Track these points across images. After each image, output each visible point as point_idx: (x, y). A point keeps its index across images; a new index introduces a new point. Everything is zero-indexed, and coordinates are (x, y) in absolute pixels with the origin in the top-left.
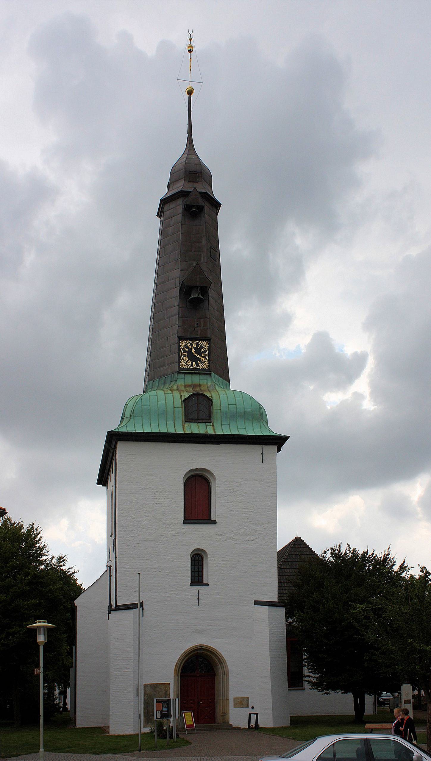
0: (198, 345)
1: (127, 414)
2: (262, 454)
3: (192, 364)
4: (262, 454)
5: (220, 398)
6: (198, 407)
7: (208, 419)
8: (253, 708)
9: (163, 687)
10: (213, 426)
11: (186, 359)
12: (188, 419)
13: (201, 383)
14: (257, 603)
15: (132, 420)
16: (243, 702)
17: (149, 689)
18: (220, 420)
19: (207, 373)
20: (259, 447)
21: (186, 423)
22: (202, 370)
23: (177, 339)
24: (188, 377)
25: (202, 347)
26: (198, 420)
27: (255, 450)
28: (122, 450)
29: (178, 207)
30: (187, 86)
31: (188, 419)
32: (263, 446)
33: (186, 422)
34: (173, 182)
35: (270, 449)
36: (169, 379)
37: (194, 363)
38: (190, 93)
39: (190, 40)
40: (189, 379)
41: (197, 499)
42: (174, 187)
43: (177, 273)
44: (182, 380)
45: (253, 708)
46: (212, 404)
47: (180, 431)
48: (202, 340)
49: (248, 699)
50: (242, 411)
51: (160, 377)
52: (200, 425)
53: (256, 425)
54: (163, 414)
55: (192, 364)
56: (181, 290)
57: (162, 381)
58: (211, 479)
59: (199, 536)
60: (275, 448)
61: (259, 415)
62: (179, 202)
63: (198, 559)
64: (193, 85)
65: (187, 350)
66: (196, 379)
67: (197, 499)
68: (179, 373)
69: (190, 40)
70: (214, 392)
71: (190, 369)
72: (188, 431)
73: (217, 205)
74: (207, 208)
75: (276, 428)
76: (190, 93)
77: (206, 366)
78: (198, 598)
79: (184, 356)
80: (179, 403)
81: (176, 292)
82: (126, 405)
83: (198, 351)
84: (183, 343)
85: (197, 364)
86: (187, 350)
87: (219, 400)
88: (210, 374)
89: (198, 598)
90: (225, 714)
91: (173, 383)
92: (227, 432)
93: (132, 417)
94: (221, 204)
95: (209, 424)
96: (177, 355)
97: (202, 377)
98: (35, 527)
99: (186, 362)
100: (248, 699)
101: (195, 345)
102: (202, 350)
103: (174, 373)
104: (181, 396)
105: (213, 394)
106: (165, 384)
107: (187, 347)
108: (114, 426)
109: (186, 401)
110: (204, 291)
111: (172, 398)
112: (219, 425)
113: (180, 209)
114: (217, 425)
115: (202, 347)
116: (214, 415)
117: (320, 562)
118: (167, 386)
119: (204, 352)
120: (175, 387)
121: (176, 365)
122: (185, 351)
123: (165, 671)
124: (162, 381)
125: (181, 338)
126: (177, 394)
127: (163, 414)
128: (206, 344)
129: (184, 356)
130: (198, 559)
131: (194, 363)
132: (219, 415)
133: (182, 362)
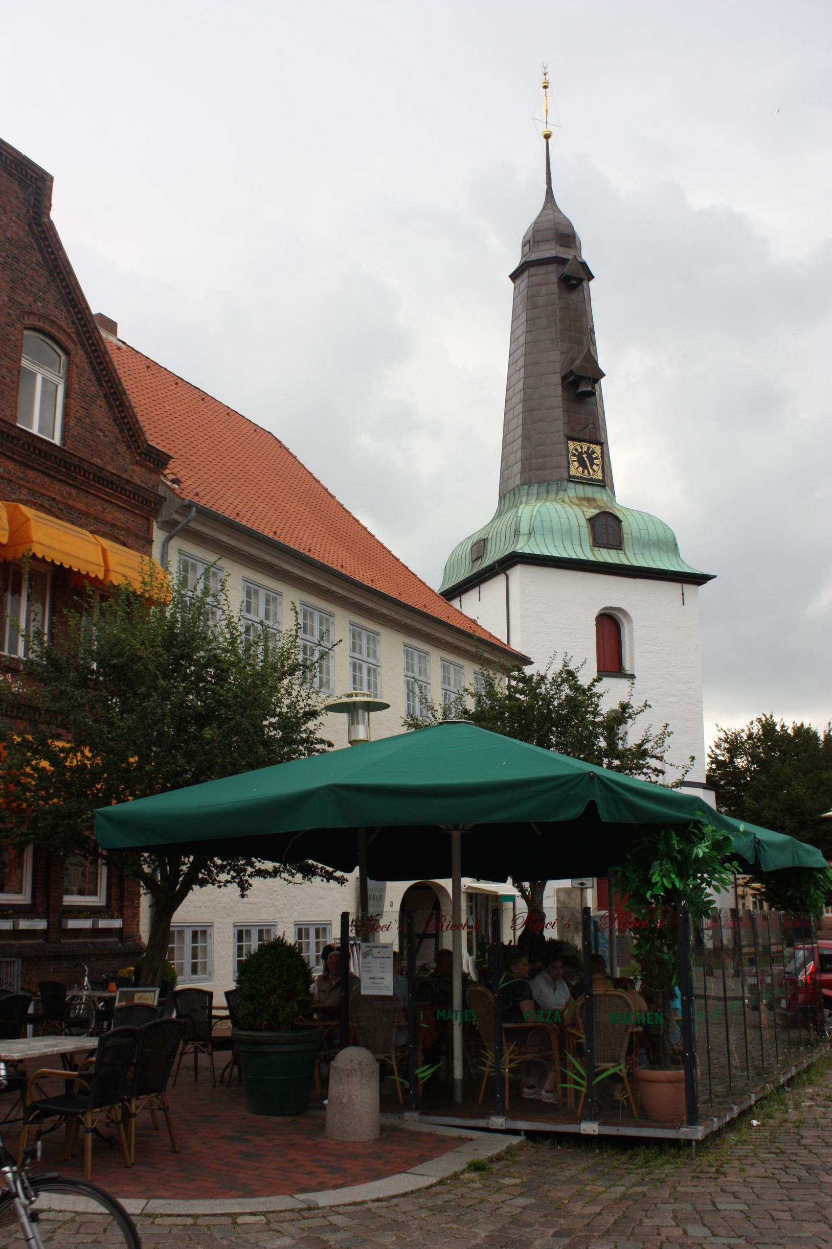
0: (588, 448)
2: (683, 594)
4: (683, 594)
7: (617, 544)
11: (576, 464)
12: (597, 543)
15: (532, 538)
17: (562, 894)
23: (563, 439)
24: (580, 487)
25: (593, 452)
27: (674, 588)
30: (543, 130)
31: (597, 543)
34: (538, 242)
36: (554, 487)
38: (547, 137)
39: (545, 74)
42: (541, 248)
43: (556, 356)
44: (575, 491)
50: (656, 539)
51: (540, 483)
53: (672, 557)
54: (567, 534)
55: (583, 472)
56: (564, 378)
57: (543, 489)
61: (671, 546)
62: (552, 268)
64: (551, 128)
68: (569, 481)
69: (545, 74)
71: (581, 478)
76: (547, 137)
80: (584, 523)
81: (557, 379)
83: (590, 455)
84: (572, 445)
94: (593, 277)
96: (564, 459)
97: (596, 489)
99: (575, 470)
101: (585, 449)
103: (561, 480)
106: (548, 492)
107: (576, 450)
113: (554, 278)
114: (629, 552)
115: (593, 452)
117: (785, 735)
118: (553, 495)
120: (567, 499)
122: (574, 455)
124: (543, 489)
125: (570, 438)
127: (567, 534)
132: (630, 541)
133: (572, 468)
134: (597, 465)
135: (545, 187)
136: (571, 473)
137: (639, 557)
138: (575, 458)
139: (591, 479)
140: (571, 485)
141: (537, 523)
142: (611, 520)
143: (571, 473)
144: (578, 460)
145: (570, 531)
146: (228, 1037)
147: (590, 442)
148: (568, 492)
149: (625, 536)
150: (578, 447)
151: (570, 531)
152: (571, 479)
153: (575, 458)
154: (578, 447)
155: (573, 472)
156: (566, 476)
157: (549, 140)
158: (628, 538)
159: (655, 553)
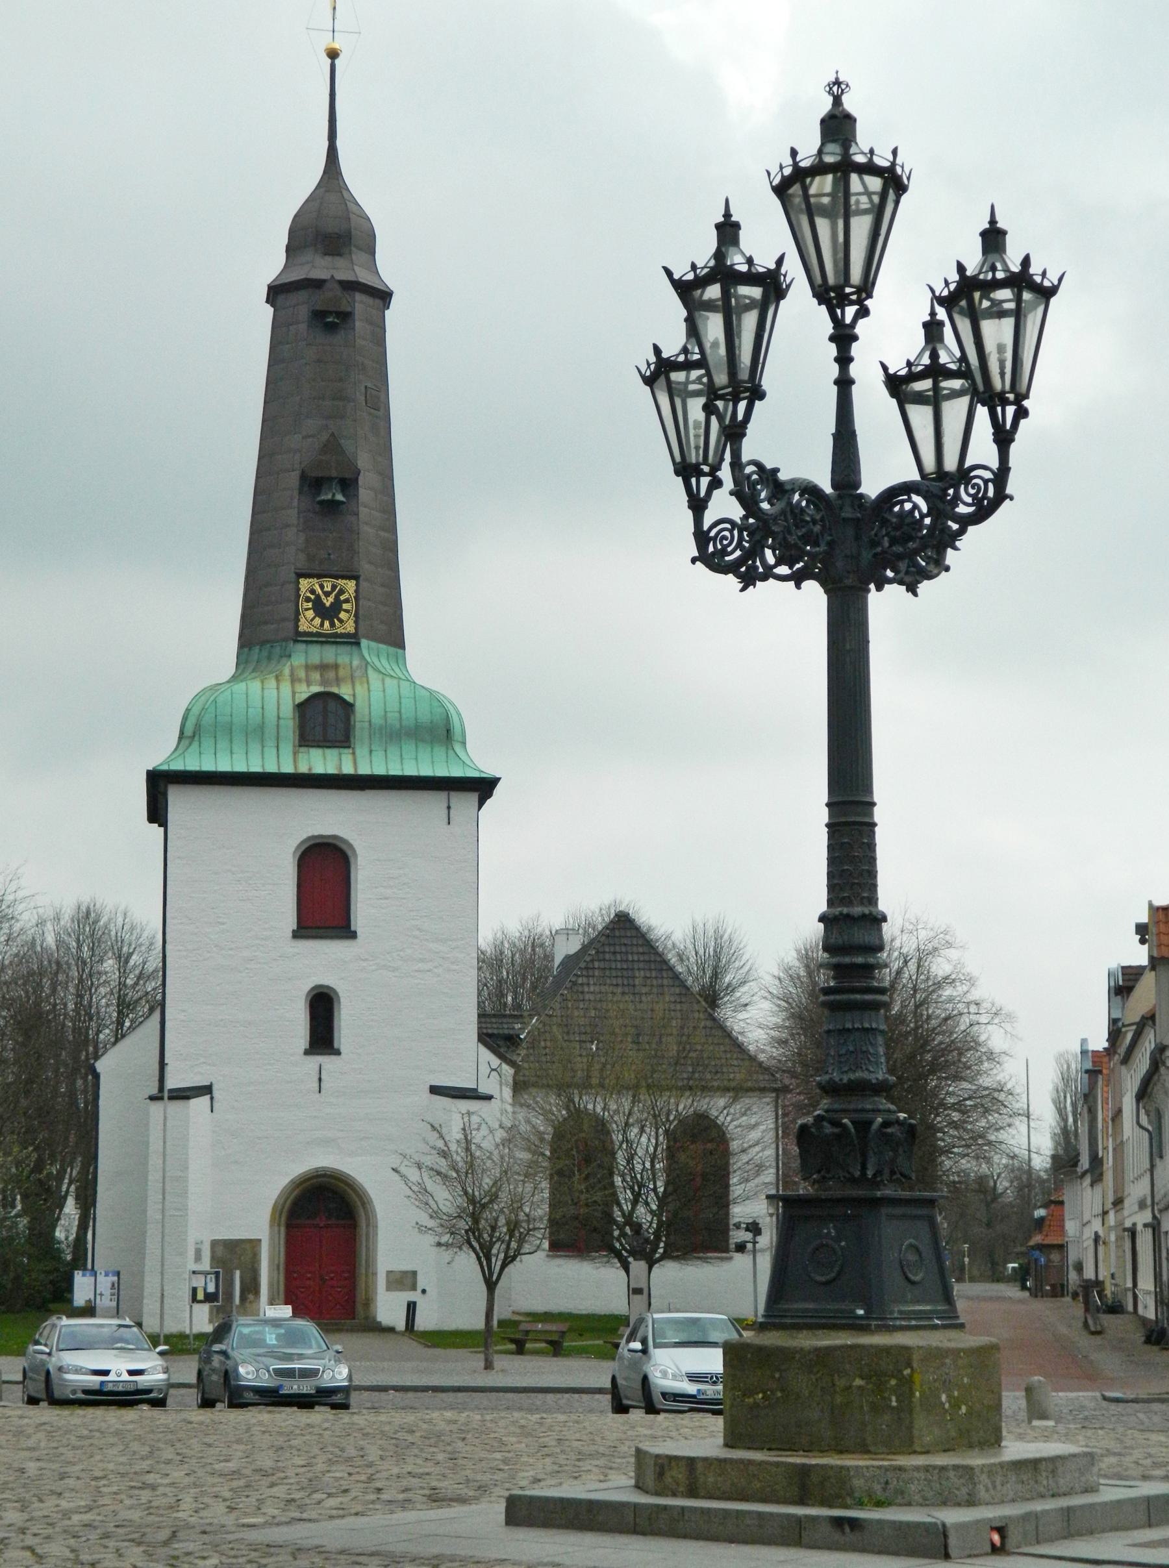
1: (189, 731)
2: (449, 808)
3: (322, 625)
4: (449, 808)
5: (372, 693)
6: (326, 720)
8: (424, 1291)
9: (248, 1246)
10: (354, 753)
13: (340, 661)
14: (435, 1090)
15: (195, 744)
16: (405, 1280)
17: (220, 1251)
18: (367, 741)
19: (352, 641)
20: (443, 795)
21: (302, 749)
22: (342, 635)
25: (342, 592)
26: (326, 742)
27: (433, 803)
28: (178, 800)
29: (302, 306)
30: (326, 41)
32: (452, 794)
33: (300, 746)
35: (464, 802)
37: (327, 624)
38: (333, 55)
40: (316, 654)
41: (324, 891)
44: (300, 656)
45: (424, 1291)
46: (353, 711)
47: (288, 768)
48: (343, 577)
49: (414, 1273)
51: (263, 643)
52: (328, 751)
53: (440, 752)
54: (257, 732)
55: (322, 625)
57: (265, 653)
58: (349, 853)
59: (323, 962)
60: (474, 797)
61: (442, 732)
62: (302, 295)
63: (322, 1005)
65: (313, 597)
66: (329, 654)
67: (324, 891)
68: (296, 641)
70: (361, 684)
71: (318, 634)
72: (303, 769)
73: (384, 296)
74: (361, 304)
75: (478, 759)
76: (333, 55)
77: (350, 627)
78: (320, 1080)
79: (307, 609)
80: (288, 710)
82: (188, 710)
84: (304, 584)
85: (332, 625)
86: (313, 597)
87: (367, 704)
88: (358, 644)
89: (320, 1080)
90: (369, 1302)
91: (284, 660)
92: (380, 770)
93: (196, 738)
95: (346, 751)
96: (292, 605)
97: (342, 649)
98: (720, 925)
99: (309, 621)
100: (414, 1273)
102: (342, 598)
103: (285, 640)
104: (294, 693)
105: (360, 690)
106: (269, 658)
107: (313, 592)
108: (161, 752)
109: (302, 708)
110: (349, 484)
111: (277, 695)
112: (366, 751)
113: (303, 312)
114: (361, 751)
116: (358, 733)
119: (347, 601)
121: (290, 625)
122: (308, 600)
123: (253, 1216)
124: (265, 653)
126: (286, 688)
127: (257, 732)
128: (350, 586)
129: (307, 609)
130: (322, 1005)
131: (327, 624)
133: (302, 620)
134: (347, 611)
135: (325, 144)
136: (301, 629)
137: (378, 756)
138: (310, 605)
139: (336, 635)
140: (301, 647)
141: (208, 719)
142: (332, 705)
143: (301, 629)
144: (314, 608)
145: (261, 728)
146: (725, 1354)
147: (337, 577)
148: (292, 659)
149: (358, 725)
150: (317, 588)
151: (261, 728)
152: (300, 637)
153: (310, 605)
154: (317, 588)
155: (304, 626)
156: (291, 634)
157: (337, 61)
158: (362, 729)
159: (409, 747)
